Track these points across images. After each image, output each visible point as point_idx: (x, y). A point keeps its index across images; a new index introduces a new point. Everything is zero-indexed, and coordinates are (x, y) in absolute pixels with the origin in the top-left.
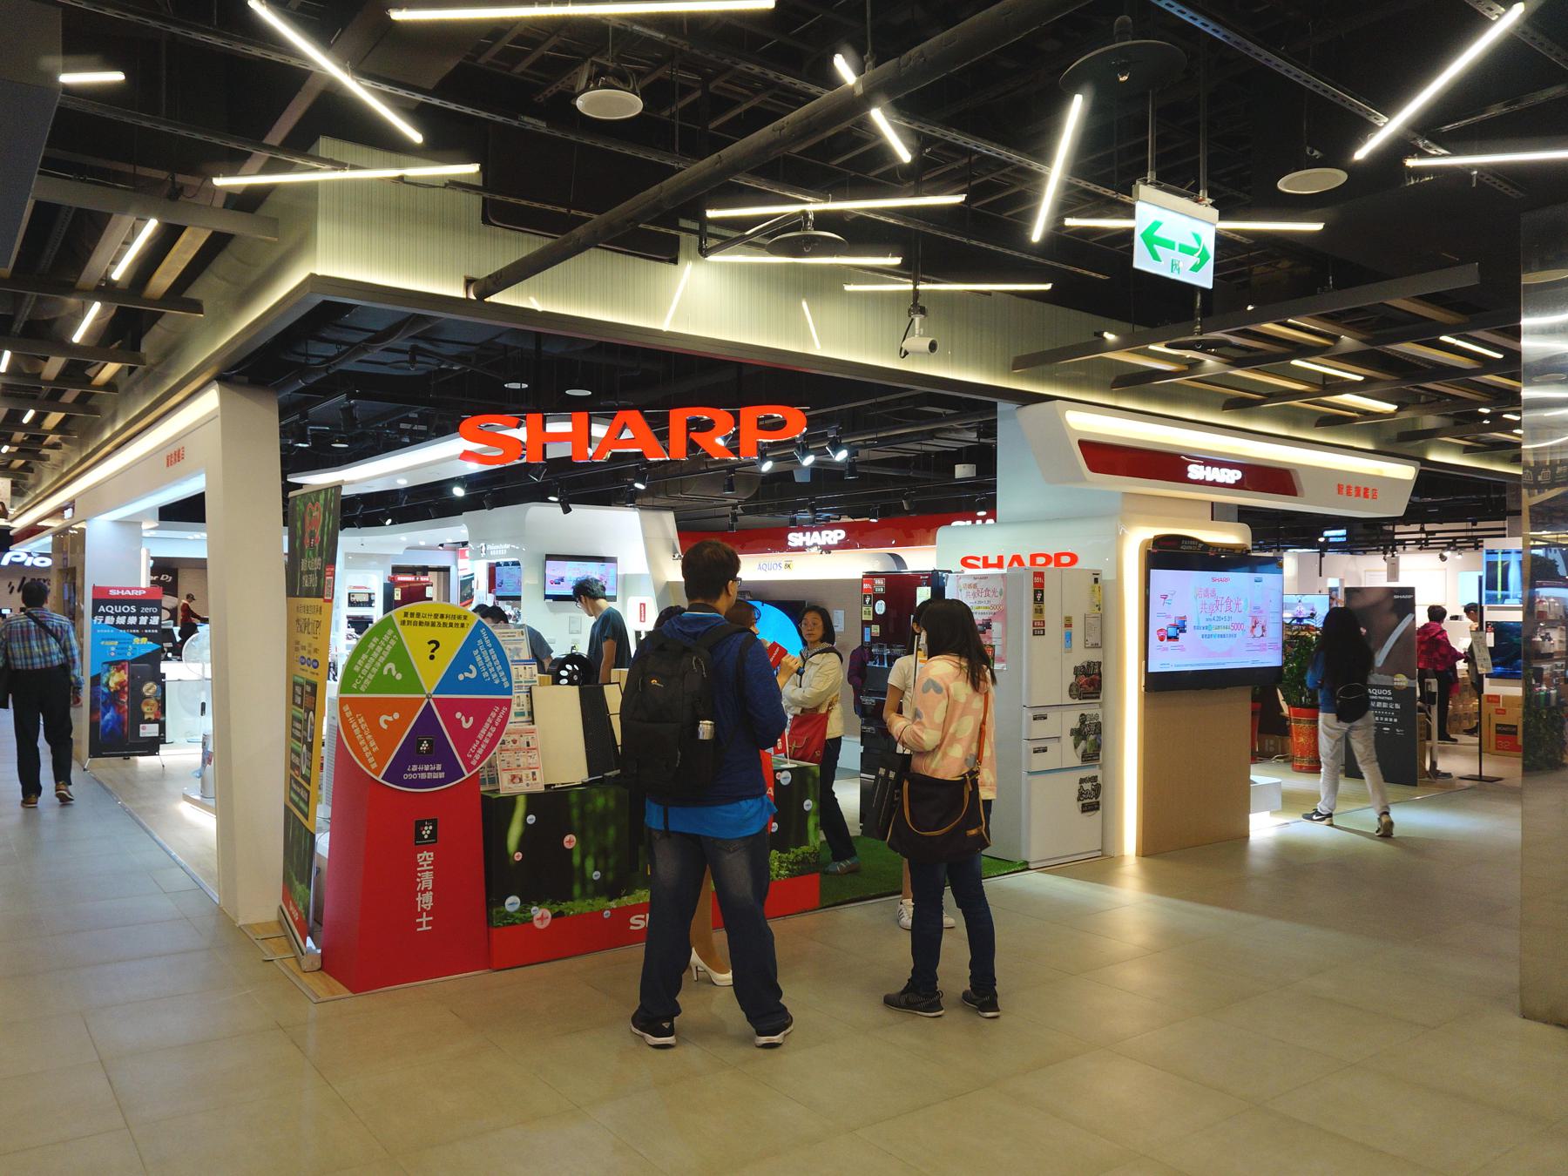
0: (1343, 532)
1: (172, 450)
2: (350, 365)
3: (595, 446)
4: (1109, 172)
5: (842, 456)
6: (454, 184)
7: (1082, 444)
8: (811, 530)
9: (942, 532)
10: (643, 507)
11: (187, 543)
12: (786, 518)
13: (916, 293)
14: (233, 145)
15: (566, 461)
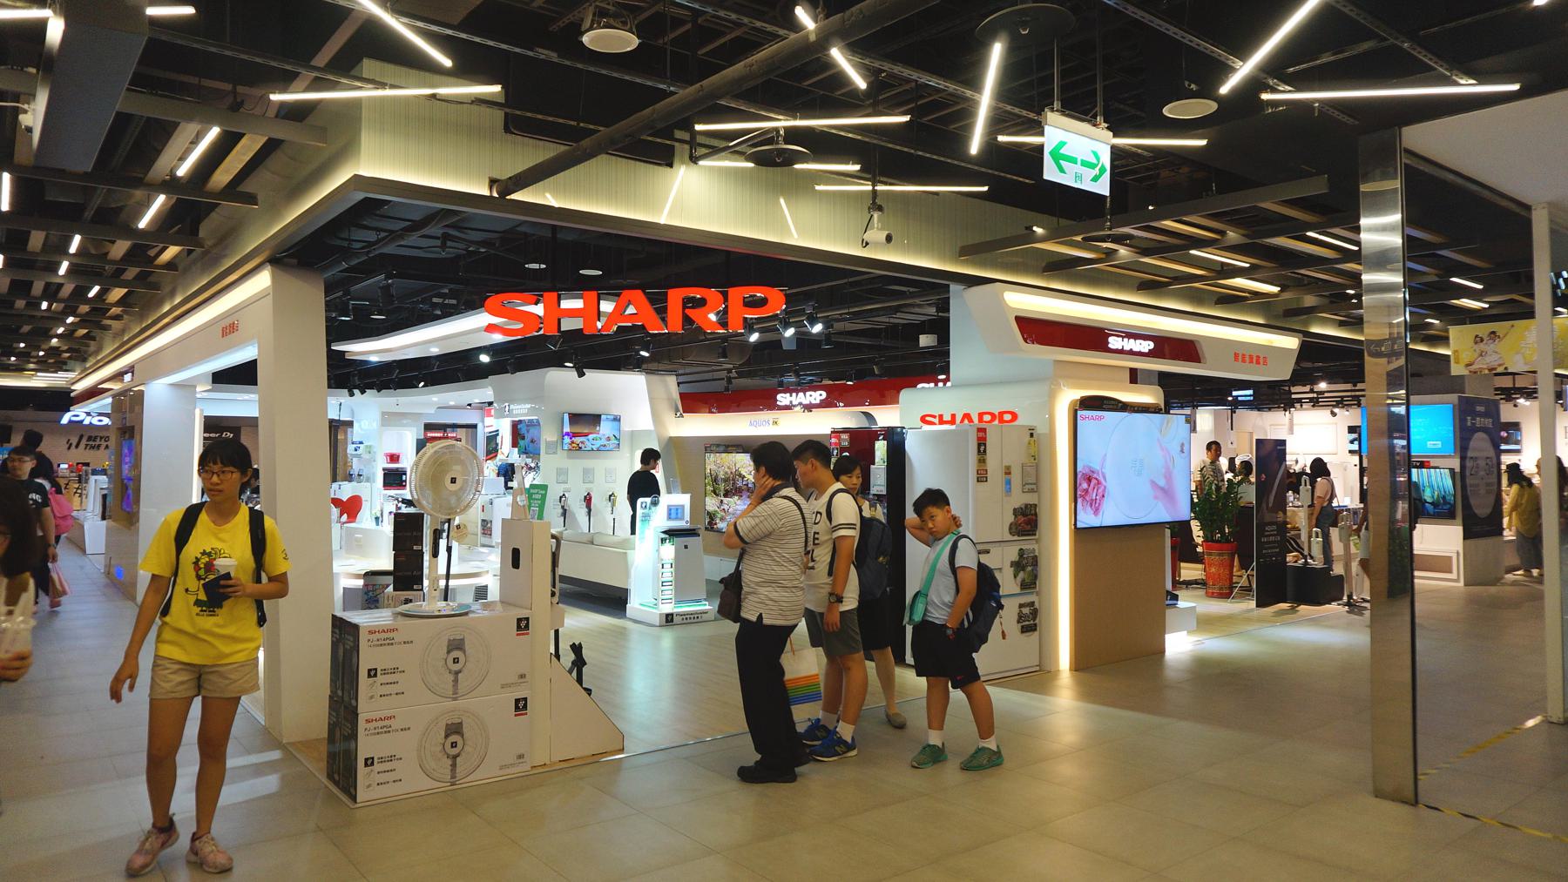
0: (1250, 392)
1: (228, 322)
2: (390, 249)
3: (604, 319)
4: (1027, 98)
5: (818, 328)
6: (479, 101)
7: (1017, 319)
8: (797, 392)
9: (905, 394)
10: (649, 372)
11: (239, 404)
12: (772, 381)
13: (874, 192)
14: (288, 67)
15: (577, 333)
